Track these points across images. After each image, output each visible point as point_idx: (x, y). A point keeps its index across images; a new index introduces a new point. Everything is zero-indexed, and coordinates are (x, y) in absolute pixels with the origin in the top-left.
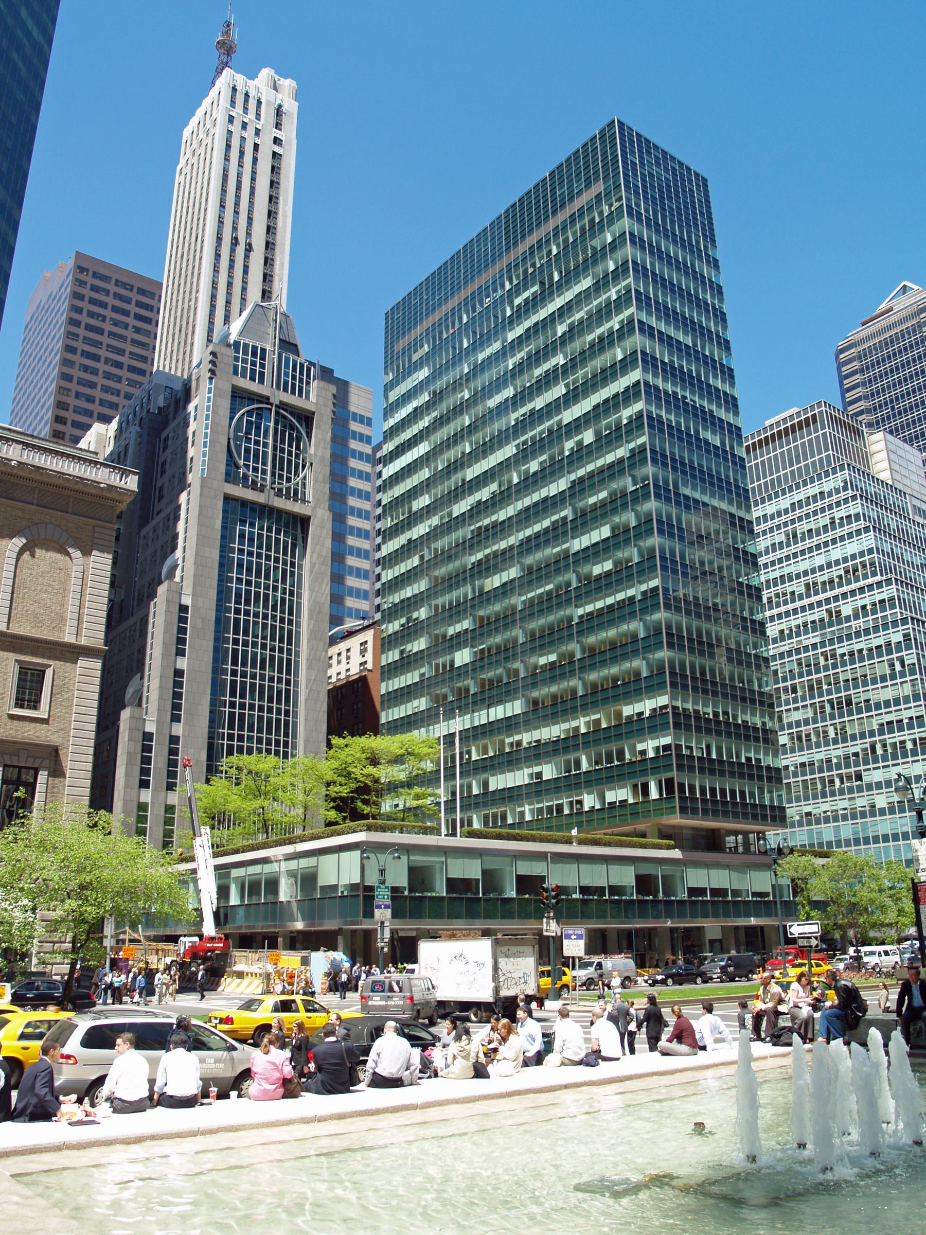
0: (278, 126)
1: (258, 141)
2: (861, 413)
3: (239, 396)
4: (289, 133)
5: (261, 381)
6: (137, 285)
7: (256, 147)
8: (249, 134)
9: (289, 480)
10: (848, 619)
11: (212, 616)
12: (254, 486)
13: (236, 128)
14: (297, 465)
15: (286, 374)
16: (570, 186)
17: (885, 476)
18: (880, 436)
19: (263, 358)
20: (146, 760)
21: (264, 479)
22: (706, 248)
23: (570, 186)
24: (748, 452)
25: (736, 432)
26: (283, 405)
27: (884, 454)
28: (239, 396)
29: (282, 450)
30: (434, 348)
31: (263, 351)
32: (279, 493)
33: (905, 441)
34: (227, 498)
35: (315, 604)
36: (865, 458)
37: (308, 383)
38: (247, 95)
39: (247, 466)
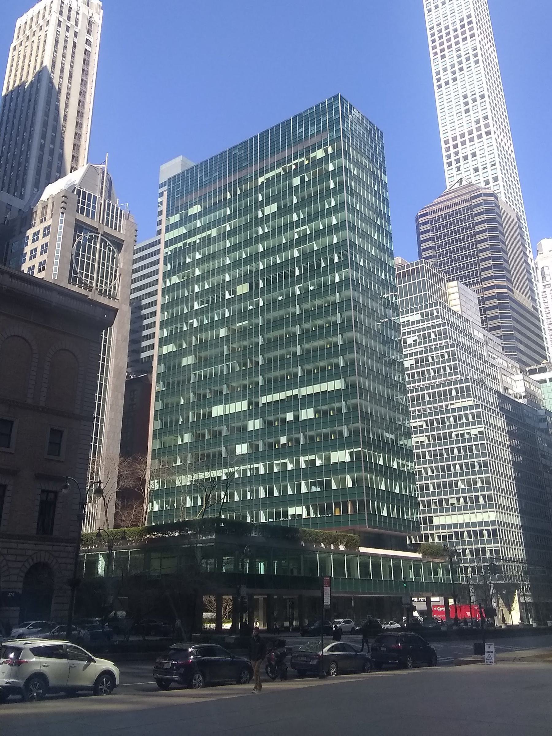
0: (89, 32)
1: (76, 40)
2: (430, 257)
3: (80, 227)
4: (96, 38)
7: (75, 44)
8: (71, 35)
10: (410, 345)
13: (62, 29)
15: (108, 215)
16: (307, 130)
17: (457, 309)
18: (454, 283)
19: (95, 202)
22: (381, 176)
23: (307, 130)
26: (105, 234)
27: (457, 296)
28: (80, 227)
29: (103, 265)
30: (175, 266)
31: (95, 197)
32: (100, 293)
33: (467, 285)
35: (116, 366)
36: (445, 296)
37: (120, 221)
38: (70, 8)
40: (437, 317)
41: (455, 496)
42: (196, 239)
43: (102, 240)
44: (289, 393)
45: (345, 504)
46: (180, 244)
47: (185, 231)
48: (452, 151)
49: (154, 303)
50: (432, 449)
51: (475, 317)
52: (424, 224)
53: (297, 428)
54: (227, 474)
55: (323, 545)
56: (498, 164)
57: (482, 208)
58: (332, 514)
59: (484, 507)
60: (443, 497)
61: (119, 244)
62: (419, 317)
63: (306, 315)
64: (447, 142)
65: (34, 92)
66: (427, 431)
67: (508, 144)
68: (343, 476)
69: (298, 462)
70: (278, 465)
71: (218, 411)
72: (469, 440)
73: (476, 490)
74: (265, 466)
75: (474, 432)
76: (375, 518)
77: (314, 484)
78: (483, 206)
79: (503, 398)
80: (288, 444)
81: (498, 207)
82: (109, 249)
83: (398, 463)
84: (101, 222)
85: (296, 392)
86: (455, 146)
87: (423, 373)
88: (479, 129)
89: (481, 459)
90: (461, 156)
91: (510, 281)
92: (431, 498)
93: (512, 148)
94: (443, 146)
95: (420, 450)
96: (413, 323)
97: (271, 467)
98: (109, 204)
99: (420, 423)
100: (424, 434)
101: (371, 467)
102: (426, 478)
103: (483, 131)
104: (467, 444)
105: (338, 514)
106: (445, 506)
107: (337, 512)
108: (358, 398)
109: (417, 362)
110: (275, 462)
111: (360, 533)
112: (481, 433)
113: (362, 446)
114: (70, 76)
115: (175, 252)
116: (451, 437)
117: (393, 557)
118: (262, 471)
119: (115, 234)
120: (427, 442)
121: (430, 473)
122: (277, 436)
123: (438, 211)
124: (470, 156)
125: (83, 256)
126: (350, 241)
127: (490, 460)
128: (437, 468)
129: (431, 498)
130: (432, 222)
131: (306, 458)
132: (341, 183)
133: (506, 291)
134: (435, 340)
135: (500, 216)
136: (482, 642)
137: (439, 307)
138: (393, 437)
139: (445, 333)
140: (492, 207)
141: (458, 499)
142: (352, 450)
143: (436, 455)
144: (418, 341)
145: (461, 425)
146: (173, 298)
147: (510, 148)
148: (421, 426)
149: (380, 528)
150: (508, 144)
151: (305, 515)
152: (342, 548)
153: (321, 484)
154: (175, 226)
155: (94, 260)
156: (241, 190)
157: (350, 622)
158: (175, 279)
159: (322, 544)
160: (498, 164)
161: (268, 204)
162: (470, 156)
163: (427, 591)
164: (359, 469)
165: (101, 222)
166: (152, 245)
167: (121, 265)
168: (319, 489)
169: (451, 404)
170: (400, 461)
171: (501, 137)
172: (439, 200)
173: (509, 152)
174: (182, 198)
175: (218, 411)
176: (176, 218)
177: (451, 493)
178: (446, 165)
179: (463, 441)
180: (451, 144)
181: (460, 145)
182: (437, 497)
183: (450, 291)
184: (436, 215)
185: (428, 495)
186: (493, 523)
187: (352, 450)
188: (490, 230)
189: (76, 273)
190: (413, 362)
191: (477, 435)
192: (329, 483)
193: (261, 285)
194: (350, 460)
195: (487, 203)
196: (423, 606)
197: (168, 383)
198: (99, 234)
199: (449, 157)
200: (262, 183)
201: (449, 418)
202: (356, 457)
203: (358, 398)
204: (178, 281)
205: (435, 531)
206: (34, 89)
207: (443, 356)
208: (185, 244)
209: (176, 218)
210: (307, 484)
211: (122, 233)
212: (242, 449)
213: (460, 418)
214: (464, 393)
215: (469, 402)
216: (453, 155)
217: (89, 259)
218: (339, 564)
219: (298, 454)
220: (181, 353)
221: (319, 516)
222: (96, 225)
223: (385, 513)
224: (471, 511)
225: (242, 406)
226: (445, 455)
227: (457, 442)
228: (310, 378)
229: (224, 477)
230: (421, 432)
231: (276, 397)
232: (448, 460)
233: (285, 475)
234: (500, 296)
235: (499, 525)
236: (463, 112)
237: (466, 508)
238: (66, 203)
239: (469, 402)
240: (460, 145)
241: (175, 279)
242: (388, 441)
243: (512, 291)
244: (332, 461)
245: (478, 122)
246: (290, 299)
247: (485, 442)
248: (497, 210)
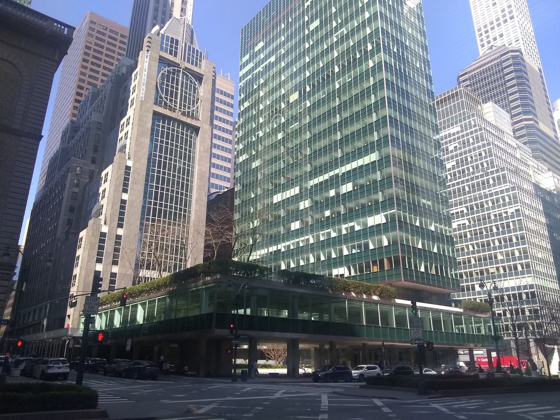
3: (162, 60)
5: (176, 55)
6: (120, 32)
9: (189, 108)
10: (452, 151)
11: (144, 173)
12: (171, 109)
14: (194, 101)
20: (101, 248)
21: (176, 106)
24: (438, 104)
25: (431, 94)
30: (246, 96)
31: (177, 41)
32: (183, 114)
34: (155, 113)
35: (200, 170)
37: (200, 61)
39: (167, 99)
40: (475, 126)
41: (495, 266)
42: (260, 69)
44: (332, 173)
45: (382, 262)
46: (250, 76)
47: (253, 65)
48: (484, 35)
50: (472, 229)
51: (508, 128)
52: (464, 81)
53: (338, 202)
54: (284, 247)
55: (353, 294)
56: (521, 39)
57: (510, 62)
58: (370, 271)
59: (522, 273)
60: (484, 268)
61: (199, 78)
62: (459, 129)
63: (343, 106)
64: (479, 30)
66: (467, 214)
67: (528, 26)
68: (379, 237)
69: (340, 231)
70: (323, 235)
71: (277, 198)
72: (507, 218)
73: (514, 259)
74: (313, 237)
75: (510, 211)
76: (410, 274)
77: (353, 247)
78: (511, 60)
79: (537, 186)
80: (332, 216)
81: (523, 60)
82: (191, 82)
83: (436, 227)
85: (337, 171)
86: (487, 32)
87: (464, 171)
88: (504, 16)
89: (518, 233)
90: (491, 39)
91: (536, 116)
92: (473, 269)
93: (531, 28)
94: (477, 33)
95: (462, 231)
96: (454, 134)
97: (318, 237)
98: (190, 47)
99: (461, 209)
100: (465, 218)
101: (403, 225)
102: (468, 254)
103: (508, 16)
104: (504, 222)
105: (375, 270)
106: (485, 274)
107: (376, 269)
108: (392, 165)
109: (457, 163)
110: (321, 233)
111: (398, 287)
112: (517, 211)
113: (396, 208)
115: (246, 84)
116: (489, 218)
117: (431, 309)
118: (311, 241)
120: (467, 224)
121: (471, 249)
122: (322, 211)
123: (474, 70)
124: (498, 37)
125: (167, 85)
126: (385, 62)
127: (526, 233)
128: (477, 244)
129: (473, 269)
130: (470, 79)
131: (346, 226)
132: (378, 45)
133: (532, 122)
134: (473, 143)
135: (525, 67)
136: (101, 334)
137: (476, 117)
138: (430, 203)
139: (482, 137)
140: (518, 60)
141: (498, 269)
142: (387, 213)
143: (476, 234)
144: (458, 146)
145: (499, 206)
146: (245, 119)
147: (530, 28)
148: (462, 212)
149: (417, 282)
150: (528, 26)
151: (347, 274)
152: (375, 298)
153: (359, 247)
154: (247, 63)
155: (177, 89)
156: (292, 19)
157: (375, 368)
158: (246, 104)
159: (352, 293)
160: (521, 39)
161: (312, 22)
162: (498, 37)
163: (469, 342)
164: (394, 228)
167: (201, 94)
168: (359, 251)
169: (489, 191)
170: (438, 225)
171: (523, 20)
172: (475, 62)
173: (530, 31)
174: (251, 41)
175: (277, 198)
176: (247, 57)
177: (491, 264)
178: (480, 47)
179: (501, 220)
180: (483, 30)
181: (490, 30)
182: (478, 268)
183: (485, 111)
184: (473, 73)
185: (470, 267)
186: (531, 286)
187: (387, 213)
188: (517, 78)
189: (161, 97)
190: (454, 163)
191: (513, 213)
192: (367, 245)
193: (308, 89)
194: (385, 222)
195: (514, 57)
196: (467, 358)
197: (243, 184)
198: (181, 68)
199: (482, 40)
200: (308, 6)
201: (487, 202)
202: (391, 220)
203: (392, 165)
204: (249, 105)
205: (477, 296)
207: (480, 154)
208: (253, 75)
209: (247, 57)
210: (348, 248)
211: (204, 68)
212: (295, 225)
213: (498, 200)
214: (499, 180)
215: (503, 187)
216: (485, 39)
217: (172, 87)
218: (372, 316)
219: (339, 223)
220: (253, 158)
221: (359, 274)
222: (177, 60)
223: (423, 269)
224: (510, 278)
225: (296, 190)
226: (484, 233)
227: (496, 221)
228: (347, 158)
229: (283, 250)
230: (463, 216)
231: (321, 179)
232: (487, 236)
233: (330, 242)
234: (527, 127)
235: (536, 288)
236: (491, 5)
237: (505, 276)
238: (150, 43)
239: (503, 187)
240: (490, 30)
241: (246, 104)
242: (425, 208)
243: (537, 123)
244: (369, 225)
245: (503, 11)
246: (331, 97)
247: (522, 218)
248: (522, 62)
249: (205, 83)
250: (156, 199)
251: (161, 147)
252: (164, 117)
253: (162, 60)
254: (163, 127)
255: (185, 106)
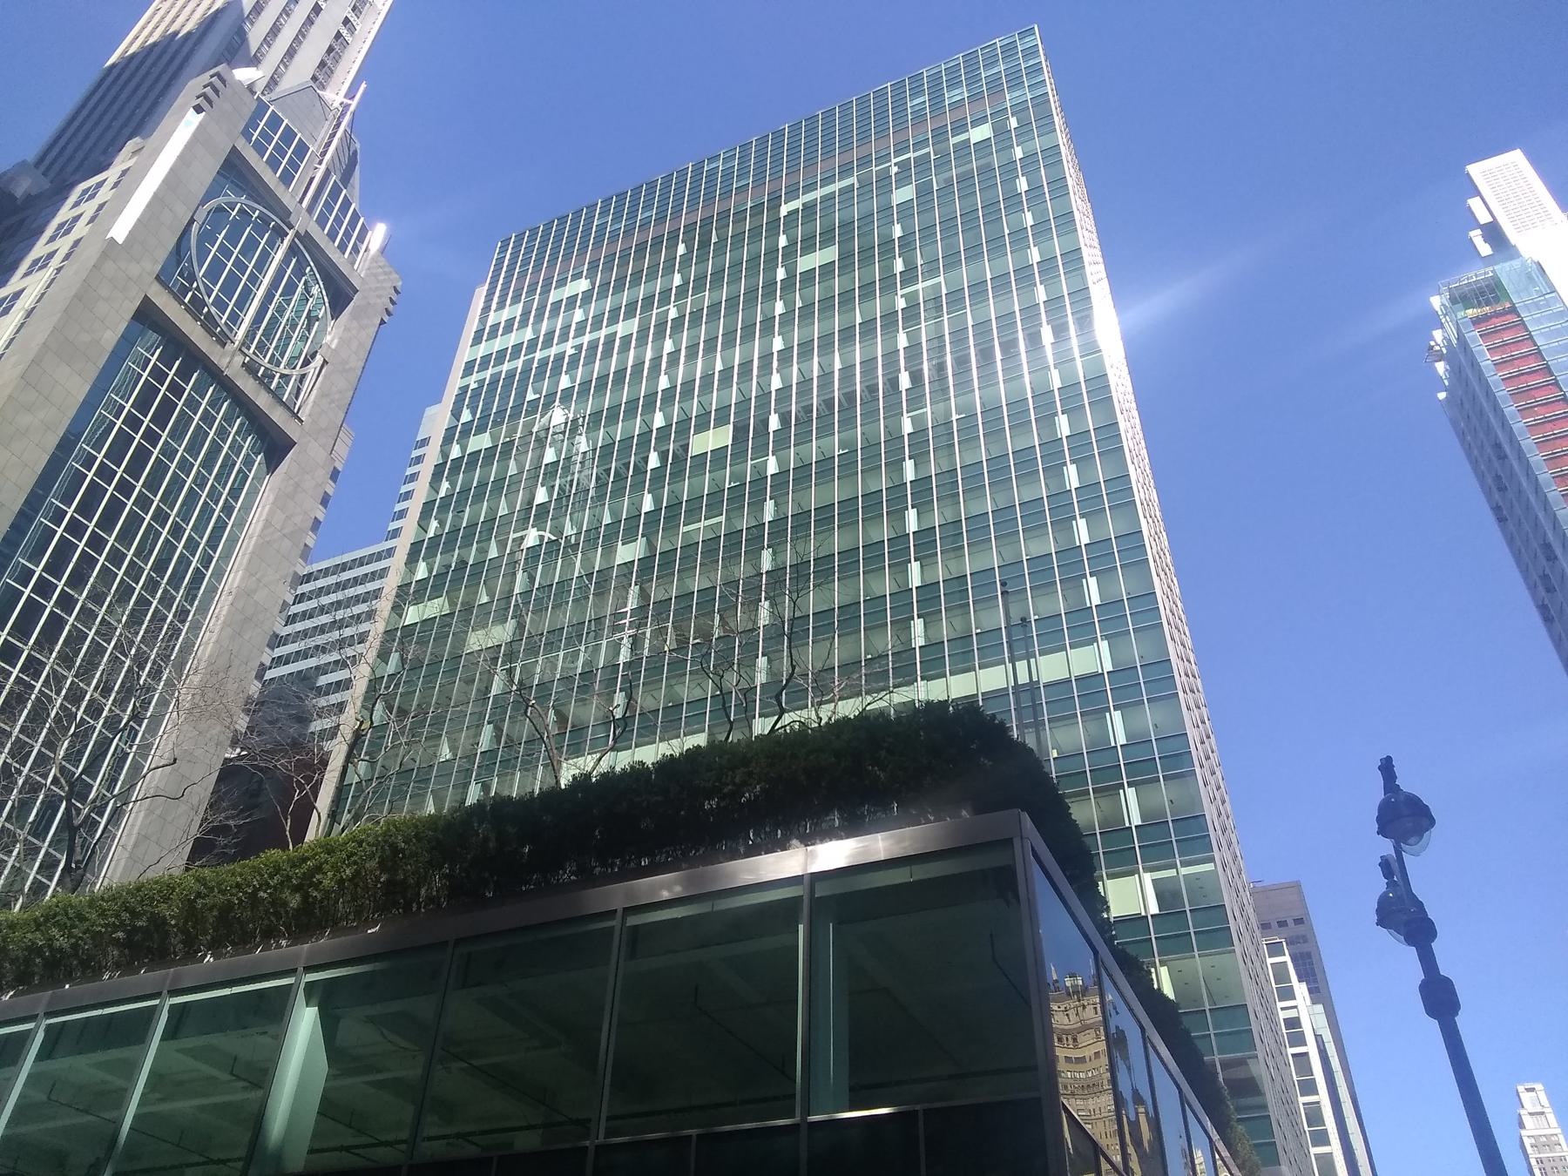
12: (209, 324)
26: (305, 238)
31: (302, 149)
34: (147, 316)
35: (244, 593)
43: (292, 250)
49: (345, 685)
65: (185, 50)
84: (305, 204)
114: (291, 53)
119: (340, 260)
165: (305, 204)
166: (379, 557)
206: (189, 44)
222: (288, 197)
238: (216, 91)
249: (354, 317)
250: (55, 568)
251: (65, 549)
252: (176, 344)
253: (234, 171)
254: (159, 375)
255: (261, 348)
